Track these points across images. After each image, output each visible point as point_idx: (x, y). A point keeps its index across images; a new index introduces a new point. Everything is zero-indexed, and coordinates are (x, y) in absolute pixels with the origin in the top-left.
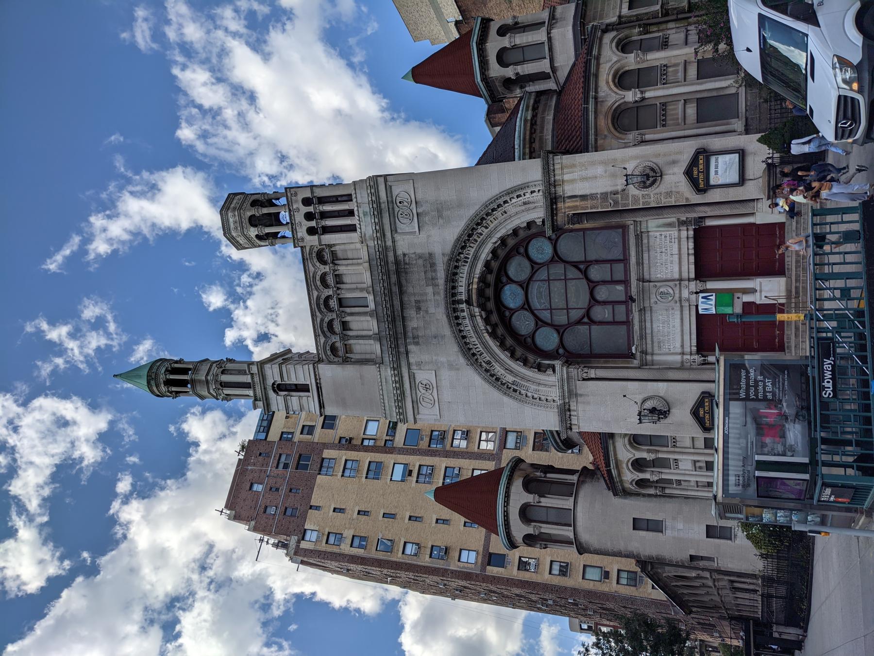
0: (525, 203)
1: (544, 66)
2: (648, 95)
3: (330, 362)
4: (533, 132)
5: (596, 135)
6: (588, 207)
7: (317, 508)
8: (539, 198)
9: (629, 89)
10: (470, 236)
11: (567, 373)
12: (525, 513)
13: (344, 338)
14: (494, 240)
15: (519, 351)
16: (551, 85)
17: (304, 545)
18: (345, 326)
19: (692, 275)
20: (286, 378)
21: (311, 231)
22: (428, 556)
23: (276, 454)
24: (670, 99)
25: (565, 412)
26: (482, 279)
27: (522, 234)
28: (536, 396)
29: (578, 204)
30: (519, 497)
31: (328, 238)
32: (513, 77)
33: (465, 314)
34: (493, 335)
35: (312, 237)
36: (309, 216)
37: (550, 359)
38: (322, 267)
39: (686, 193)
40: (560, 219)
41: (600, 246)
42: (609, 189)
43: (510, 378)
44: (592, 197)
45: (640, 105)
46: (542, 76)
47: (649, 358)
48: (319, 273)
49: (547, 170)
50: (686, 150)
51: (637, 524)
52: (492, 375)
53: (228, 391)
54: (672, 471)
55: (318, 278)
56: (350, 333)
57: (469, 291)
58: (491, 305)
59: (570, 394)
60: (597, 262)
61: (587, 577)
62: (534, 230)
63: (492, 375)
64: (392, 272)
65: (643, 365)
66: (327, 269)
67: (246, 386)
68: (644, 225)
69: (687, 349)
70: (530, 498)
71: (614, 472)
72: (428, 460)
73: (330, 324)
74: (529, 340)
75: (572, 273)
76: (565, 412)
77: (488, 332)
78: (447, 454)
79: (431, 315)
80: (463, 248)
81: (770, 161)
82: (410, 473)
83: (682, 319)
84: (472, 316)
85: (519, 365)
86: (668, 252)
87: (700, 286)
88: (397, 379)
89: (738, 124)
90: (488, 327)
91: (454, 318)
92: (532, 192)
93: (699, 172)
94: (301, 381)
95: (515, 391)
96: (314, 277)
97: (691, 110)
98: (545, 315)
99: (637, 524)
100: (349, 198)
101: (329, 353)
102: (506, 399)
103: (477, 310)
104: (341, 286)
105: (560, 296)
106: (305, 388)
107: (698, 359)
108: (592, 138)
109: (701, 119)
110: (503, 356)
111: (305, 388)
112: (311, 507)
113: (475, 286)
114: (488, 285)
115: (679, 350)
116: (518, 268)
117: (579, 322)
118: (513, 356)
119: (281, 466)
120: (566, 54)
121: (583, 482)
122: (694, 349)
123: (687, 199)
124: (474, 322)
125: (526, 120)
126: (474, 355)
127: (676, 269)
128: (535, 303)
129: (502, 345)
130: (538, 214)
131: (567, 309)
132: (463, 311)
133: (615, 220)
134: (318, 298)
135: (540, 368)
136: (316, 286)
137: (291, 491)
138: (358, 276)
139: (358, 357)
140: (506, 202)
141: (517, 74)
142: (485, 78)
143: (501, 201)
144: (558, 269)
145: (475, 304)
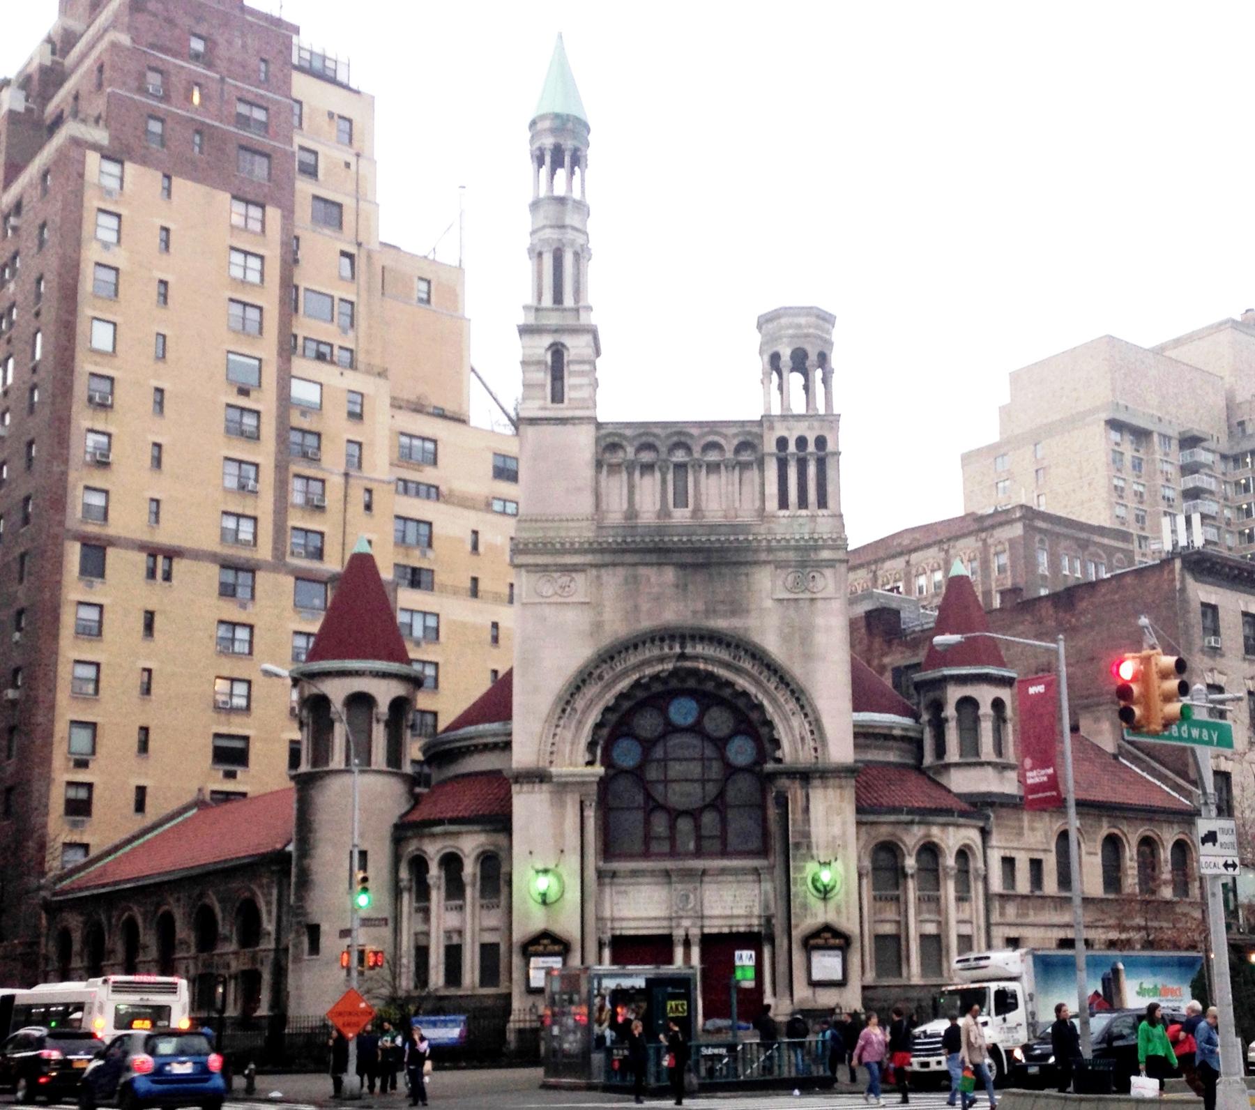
0: (803, 739)
1: (953, 755)
2: (911, 884)
3: (598, 440)
4: (876, 736)
5: (873, 823)
6: (794, 815)
7: (168, 191)
9: (917, 861)
10: (768, 666)
11: (591, 783)
12: (361, 702)
13: (630, 467)
14: (760, 696)
15: (613, 718)
16: (928, 759)
17: (93, 158)
18: (647, 468)
19: (706, 931)
20: (574, 368)
21: (782, 443)
22: (89, 424)
23: (268, 99)
24: (903, 907)
25: (538, 777)
26: (711, 676)
27: (764, 731)
29: (799, 804)
30: (384, 693)
32: (943, 715)
33: (666, 650)
34: (637, 684)
35: (774, 443)
36: (801, 442)
37: (603, 755)
38: (732, 448)
39: (805, 924)
40: (784, 782)
41: (740, 822)
42: (814, 839)
45: (899, 874)
46: (940, 750)
47: (607, 880)
48: (722, 442)
50: (850, 925)
52: (584, 681)
53: (548, 260)
54: (443, 902)
56: (637, 474)
57: (696, 658)
58: (674, 683)
59: (563, 787)
61: (838, 976)
62: (768, 746)
63: (584, 681)
65: (600, 874)
66: (729, 455)
67: (558, 297)
69: (617, 925)
70: (383, 707)
71: (438, 829)
72: (269, 429)
73: (650, 447)
74: (625, 729)
75: (712, 789)
76: (538, 777)
77: (640, 678)
78: (281, 467)
79: (667, 602)
80: (753, 656)
81: (838, 1011)
82: (244, 392)
84: (661, 660)
86: (730, 902)
87: (695, 941)
89: (870, 977)
92: (816, 750)
94: (568, 394)
95: (564, 711)
97: (888, 929)
98: (658, 753)
100: (822, 503)
101: (609, 440)
104: (704, 471)
105: (684, 776)
106: (558, 397)
107: (607, 937)
108: (872, 818)
109: (879, 939)
110: (609, 698)
111: (558, 397)
112: (168, 177)
113: (702, 666)
115: (617, 914)
116: (719, 722)
117: (649, 796)
118: (607, 710)
119: (243, 109)
120: (963, 782)
121: (405, 781)
122: (618, 932)
123: (797, 926)
124: (656, 663)
125: (891, 728)
126: (612, 658)
127: (716, 912)
128: (675, 740)
129: (621, 696)
130: (787, 751)
132: (671, 648)
133: (777, 845)
134: (691, 436)
135: (591, 746)
136: (709, 433)
137: (198, 132)
138: (720, 499)
139: (603, 484)
140: (806, 715)
141: (946, 720)
142: (946, 680)
143: (808, 710)
144: (716, 770)
145: (679, 664)
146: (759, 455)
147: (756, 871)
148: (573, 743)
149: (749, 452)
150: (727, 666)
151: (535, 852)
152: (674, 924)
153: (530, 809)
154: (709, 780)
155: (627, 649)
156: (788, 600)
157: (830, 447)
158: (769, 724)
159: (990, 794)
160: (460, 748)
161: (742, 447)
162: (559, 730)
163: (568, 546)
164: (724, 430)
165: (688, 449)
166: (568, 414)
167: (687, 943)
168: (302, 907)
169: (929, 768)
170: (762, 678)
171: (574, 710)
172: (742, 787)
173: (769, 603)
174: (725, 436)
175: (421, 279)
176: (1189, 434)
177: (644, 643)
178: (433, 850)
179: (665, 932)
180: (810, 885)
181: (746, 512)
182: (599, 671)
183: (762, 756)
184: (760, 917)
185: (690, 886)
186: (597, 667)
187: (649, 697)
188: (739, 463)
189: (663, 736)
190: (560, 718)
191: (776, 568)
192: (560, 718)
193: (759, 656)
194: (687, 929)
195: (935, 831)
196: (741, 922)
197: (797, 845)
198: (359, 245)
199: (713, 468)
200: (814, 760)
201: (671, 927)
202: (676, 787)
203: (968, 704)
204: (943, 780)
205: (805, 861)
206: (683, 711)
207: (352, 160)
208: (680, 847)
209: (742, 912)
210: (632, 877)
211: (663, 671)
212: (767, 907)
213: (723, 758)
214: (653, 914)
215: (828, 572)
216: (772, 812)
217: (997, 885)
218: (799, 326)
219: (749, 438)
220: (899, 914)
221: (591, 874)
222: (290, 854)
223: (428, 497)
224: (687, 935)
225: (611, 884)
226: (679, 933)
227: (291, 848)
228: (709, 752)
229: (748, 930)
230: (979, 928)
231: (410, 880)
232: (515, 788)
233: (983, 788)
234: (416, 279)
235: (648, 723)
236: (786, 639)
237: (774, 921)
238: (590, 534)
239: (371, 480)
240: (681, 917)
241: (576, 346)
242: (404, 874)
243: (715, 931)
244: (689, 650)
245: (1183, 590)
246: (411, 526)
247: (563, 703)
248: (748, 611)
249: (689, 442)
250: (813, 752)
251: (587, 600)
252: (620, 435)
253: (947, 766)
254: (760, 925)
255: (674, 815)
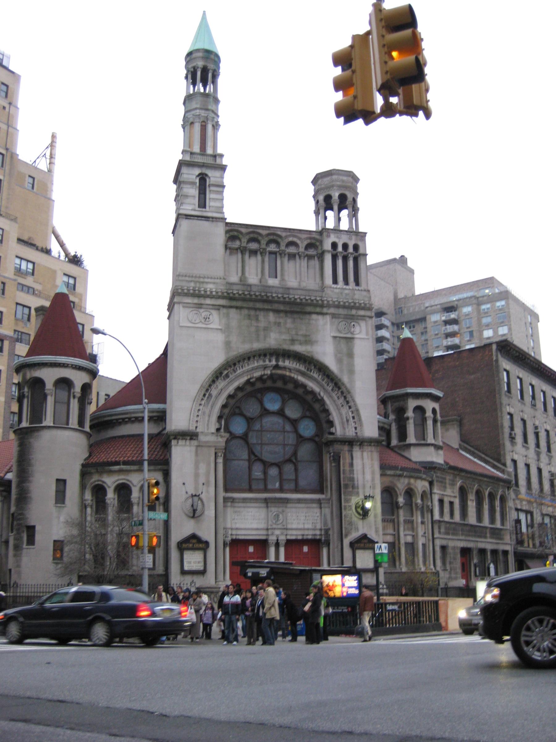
0: (348, 421)
1: (411, 439)
2: (401, 512)
8: (350, 433)
12: (64, 383)
16: (394, 442)
18: (253, 253)
20: (212, 188)
27: (323, 416)
28: (200, 412)
31: (328, 259)
32: (405, 415)
33: (267, 362)
34: (248, 382)
43: (214, 392)
44: (352, 471)
46: (403, 435)
47: (229, 504)
48: (298, 242)
49: (371, 442)
51: (61, 483)
53: (197, 127)
55: (295, 240)
57: (285, 368)
58: (269, 384)
60: (296, 470)
61: (200, 567)
62: (325, 425)
64: (298, 308)
65: (225, 499)
66: (302, 249)
68: (326, 505)
70: (78, 389)
71: (117, 468)
75: (289, 450)
77: (251, 379)
83: (257, 529)
84: (265, 368)
85: (223, 401)
86: (302, 519)
88: (214, 293)
90: (254, 380)
91: (263, 354)
92: (356, 428)
93: (194, 544)
96: (295, 236)
99: (61, 483)
100: (357, 283)
102: (198, 386)
103: (269, 372)
106: (202, 204)
110: (231, 389)
113: (288, 374)
114: (285, 383)
120: (418, 455)
122: (234, 537)
126: (235, 364)
127: (294, 526)
129: (239, 389)
130: (339, 430)
131: (262, 444)
132: (270, 361)
136: (290, 236)
138: (296, 277)
140: (350, 407)
141: (408, 418)
143: (351, 404)
146: (320, 252)
147: (319, 501)
148: (209, 416)
149: (312, 250)
150: (303, 374)
151: (182, 485)
152: (270, 533)
153: (181, 455)
154: (288, 445)
155: (244, 359)
156: (340, 337)
157: (361, 251)
158: (327, 412)
159: (432, 463)
160: (117, 420)
161: (310, 245)
162: (201, 407)
163: (208, 293)
164: (299, 235)
165: (278, 244)
166: (209, 214)
167: (277, 545)
168: (22, 514)
169: (395, 447)
170: (324, 383)
171: (210, 395)
172: (305, 451)
173: (330, 340)
174: (300, 239)
175: (30, 176)
176: (379, 311)
177: (254, 356)
178: (110, 482)
179: (264, 538)
180: (354, 511)
181: (311, 283)
182: (226, 372)
183: (320, 431)
184: (321, 530)
185: (280, 510)
186: (225, 369)
187: (254, 390)
188: (307, 255)
189: (261, 416)
190: (202, 399)
191: (332, 318)
192: (202, 399)
193: (322, 369)
194: (277, 536)
195: (412, 481)
196: (311, 532)
197: (346, 486)
198: (7, 149)
199: (292, 256)
200: (354, 434)
201: (268, 535)
202: (266, 448)
203: (420, 410)
204: (406, 454)
205: (351, 495)
206: (272, 403)
207: (7, 106)
208: (270, 487)
209: (310, 526)
210: (243, 502)
211: (264, 375)
212: (325, 524)
213: (296, 431)
214: (255, 526)
215: (363, 324)
216: (328, 466)
217: (437, 517)
218: (343, 181)
219: (313, 241)
220: (394, 531)
221: (221, 500)
222: (10, 482)
223: (28, 292)
224: (278, 540)
225: (231, 506)
226: (272, 539)
227: (9, 476)
228: (288, 427)
229: (313, 537)
230: (429, 540)
231: (92, 500)
232: (174, 442)
233: (429, 459)
234: (27, 176)
235: (252, 408)
236: (339, 361)
237: (330, 532)
238: (222, 287)
239: (5, 277)
240: (275, 529)
241: (213, 175)
242: (88, 496)
243: (294, 538)
244: (281, 363)
245: (497, 361)
246: (20, 308)
247: (205, 390)
248: (316, 342)
249: (279, 240)
250: (354, 429)
251: (220, 327)
252: (237, 231)
253: (410, 445)
254: (321, 535)
255: (266, 465)
